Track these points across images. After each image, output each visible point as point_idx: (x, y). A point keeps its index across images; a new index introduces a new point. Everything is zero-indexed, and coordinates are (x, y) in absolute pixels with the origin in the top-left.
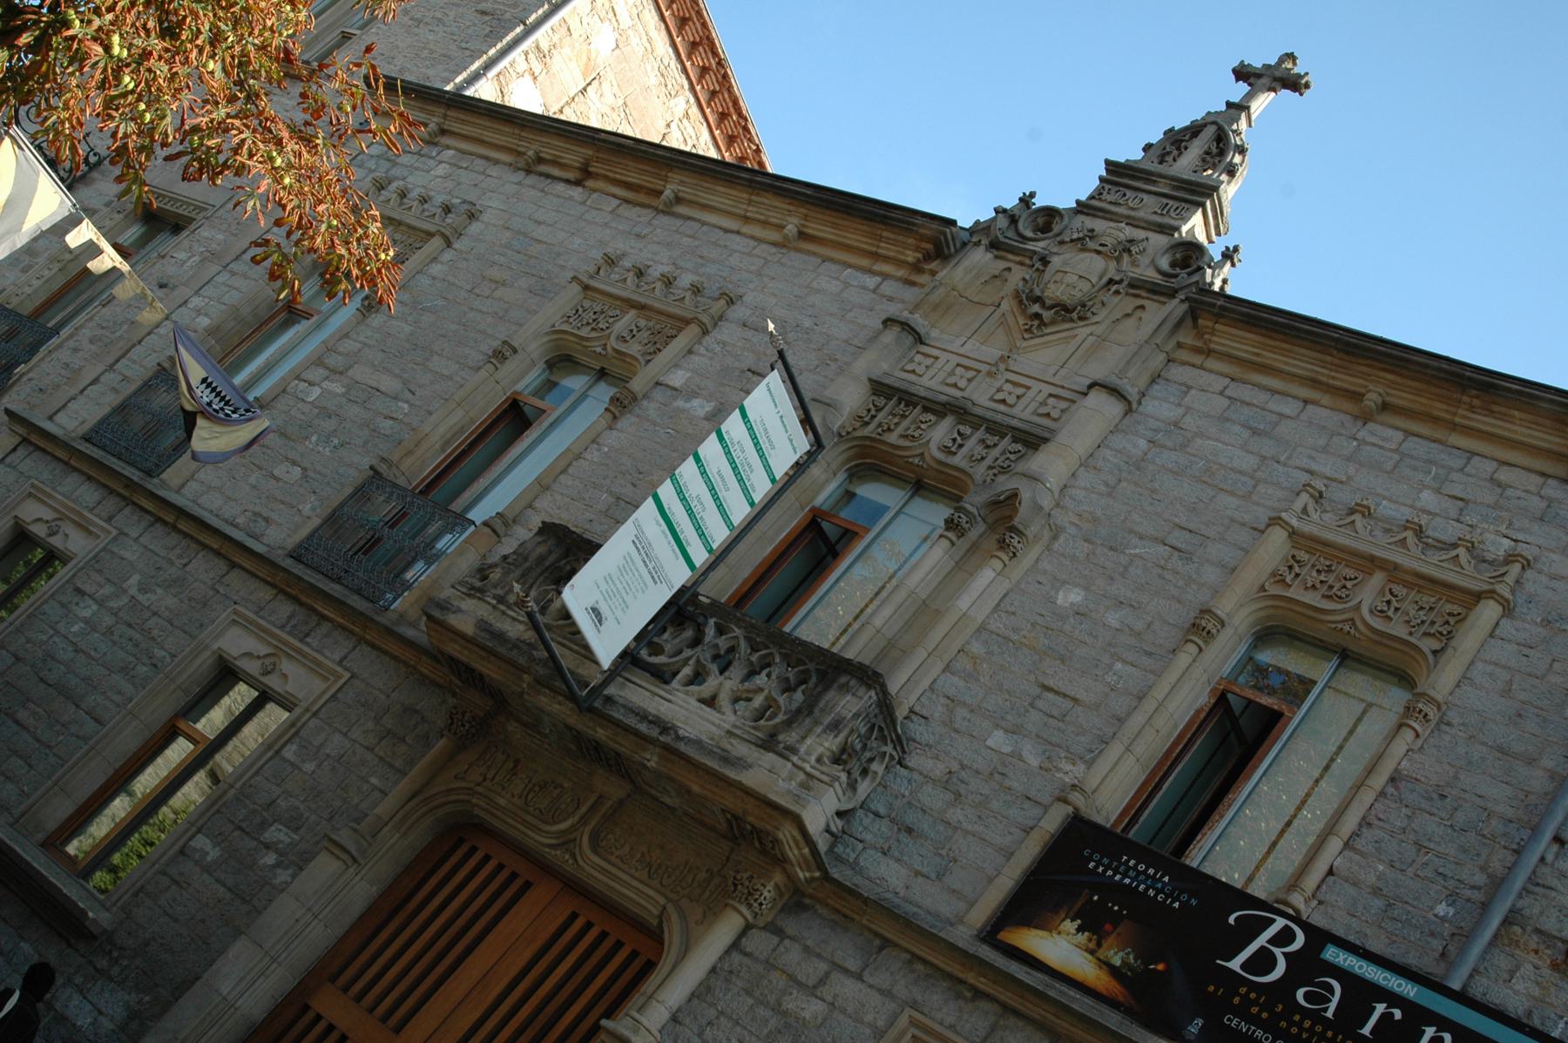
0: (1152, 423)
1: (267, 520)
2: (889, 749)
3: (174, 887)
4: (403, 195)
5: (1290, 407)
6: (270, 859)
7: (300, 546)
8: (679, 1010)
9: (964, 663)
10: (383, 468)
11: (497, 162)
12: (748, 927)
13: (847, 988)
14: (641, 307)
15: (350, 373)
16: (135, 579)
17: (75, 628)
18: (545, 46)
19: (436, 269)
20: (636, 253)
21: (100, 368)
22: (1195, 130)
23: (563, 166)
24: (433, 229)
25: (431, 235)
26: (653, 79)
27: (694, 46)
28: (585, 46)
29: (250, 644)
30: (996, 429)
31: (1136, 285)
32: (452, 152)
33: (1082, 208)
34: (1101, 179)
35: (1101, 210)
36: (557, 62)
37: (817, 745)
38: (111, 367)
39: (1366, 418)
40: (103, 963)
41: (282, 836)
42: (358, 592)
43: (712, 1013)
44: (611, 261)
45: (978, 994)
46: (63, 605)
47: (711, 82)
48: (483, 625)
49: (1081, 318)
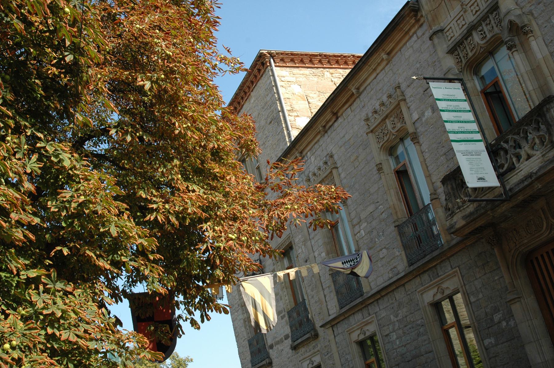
6: (504, 324)
7: (408, 262)
10: (397, 223)
11: (318, 140)
14: (386, 117)
15: (362, 218)
17: (398, 343)
18: (289, 108)
19: (343, 175)
21: (322, 293)
24: (329, 171)
25: (331, 172)
26: (315, 79)
27: (311, 61)
28: (295, 96)
29: (431, 293)
30: (484, 18)
36: (296, 107)
38: (323, 289)
41: (499, 316)
42: (432, 251)
44: (367, 120)
46: (389, 343)
47: (325, 61)
48: (464, 218)
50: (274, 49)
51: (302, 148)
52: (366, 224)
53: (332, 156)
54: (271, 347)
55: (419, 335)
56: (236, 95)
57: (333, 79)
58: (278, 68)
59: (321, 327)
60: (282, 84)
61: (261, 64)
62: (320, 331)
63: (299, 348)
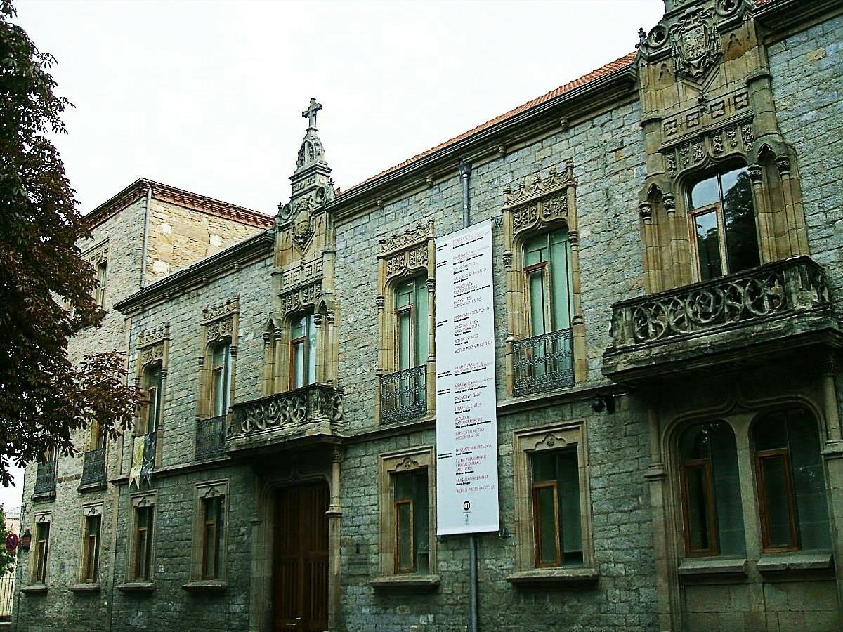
0: (341, 251)
1: (185, 455)
2: (338, 395)
3: (662, 509)
4: (149, 334)
5: (366, 220)
6: (245, 537)
8: (340, 495)
9: (341, 357)
11: (162, 304)
12: (340, 464)
13: (365, 460)
14: (221, 319)
15: (174, 398)
16: (170, 498)
17: (168, 522)
18: (151, 249)
19: (171, 350)
20: (208, 303)
21: (121, 449)
22: (303, 146)
23: (178, 292)
24: (161, 339)
25: (163, 341)
26: (190, 223)
27: (192, 203)
28: (162, 236)
29: (206, 490)
30: (311, 285)
31: (316, 212)
32: (151, 310)
33: (293, 198)
34: (292, 184)
35: (297, 195)
36: (159, 249)
37: (315, 413)
38: (123, 447)
39: (382, 208)
40: (232, 594)
41: (244, 530)
43: (346, 490)
44: (206, 312)
45: (389, 438)
46: (161, 519)
47: (207, 205)
48: (224, 509)
49: (311, 234)
50: (156, 178)
51: (146, 302)
52: (175, 405)
53: (168, 327)
54: (60, 481)
55: (186, 522)
56: (96, 211)
57: (209, 228)
58: (154, 201)
59: (113, 482)
60: (153, 219)
61: (138, 190)
62: (110, 486)
63: (86, 493)
